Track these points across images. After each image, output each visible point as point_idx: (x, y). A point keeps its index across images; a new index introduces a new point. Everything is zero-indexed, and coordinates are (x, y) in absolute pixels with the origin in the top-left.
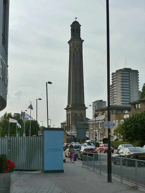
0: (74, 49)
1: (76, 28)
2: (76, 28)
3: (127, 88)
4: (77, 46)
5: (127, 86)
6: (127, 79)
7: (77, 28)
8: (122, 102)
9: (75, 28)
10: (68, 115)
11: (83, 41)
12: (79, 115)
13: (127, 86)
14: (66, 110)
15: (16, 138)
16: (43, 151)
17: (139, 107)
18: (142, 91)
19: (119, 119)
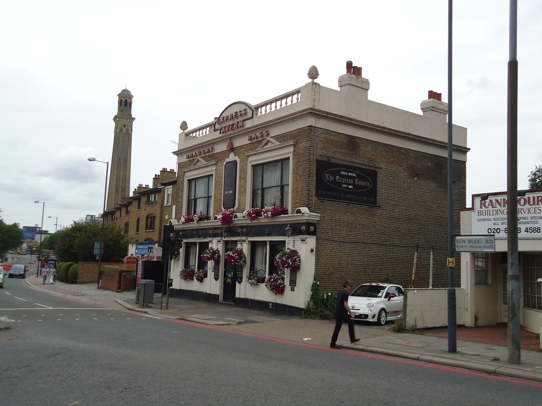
0: (119, 131)
2: (125, 101)
4: (125, 126)
7: (126, 100)
9: (124, 100)
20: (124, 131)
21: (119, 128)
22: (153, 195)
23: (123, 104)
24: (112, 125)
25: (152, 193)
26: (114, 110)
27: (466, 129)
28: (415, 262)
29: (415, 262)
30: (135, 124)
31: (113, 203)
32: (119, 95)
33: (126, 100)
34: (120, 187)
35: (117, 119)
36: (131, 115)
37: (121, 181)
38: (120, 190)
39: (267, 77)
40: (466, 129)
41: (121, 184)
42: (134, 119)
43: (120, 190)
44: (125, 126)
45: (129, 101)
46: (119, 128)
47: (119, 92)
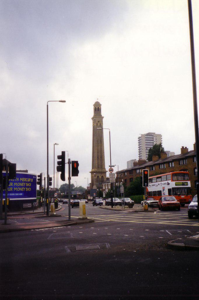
0: (96, 124)
1: (97, 109)
2: (97, 109)
3: (152, 140)
4: (99, 122)
5: (151, 139)
6: (151, 138)
7: (98, 107)
8: (146, 144)
9: (97, 108)
10: (92, 178)
11: (103, 117)
12: (100, 177)
13: (151, 139)
14: (90, 173)
15: (108, 189)
16: (18, 214)
17: (173, 166)
18: (133, 201)
19: (146, 160)
20: (99, 125)
21: (96, 123)
22: (163, 165)
23: (97, 109)
24: (91, 122)
25: (161, 164)
26: (92, 114)
27: (62, 152)
28: (29, 223)
29: (29, 223)
30: (104, 120)
31: (97, 164)
32: (94, 105)
33: (98, 107)
34: (99, 156)
35: (95, 118)
36: (101, 116)
37: (100, 152)
38: (99, 157)
39: (95, 102)
40: (62, 152)
41: (100, 154)
42: (103, 117)
43: (99, 157)
44: (99, 122)
45: (99, 108)
46: (96, 123)
47: (94, 103)
